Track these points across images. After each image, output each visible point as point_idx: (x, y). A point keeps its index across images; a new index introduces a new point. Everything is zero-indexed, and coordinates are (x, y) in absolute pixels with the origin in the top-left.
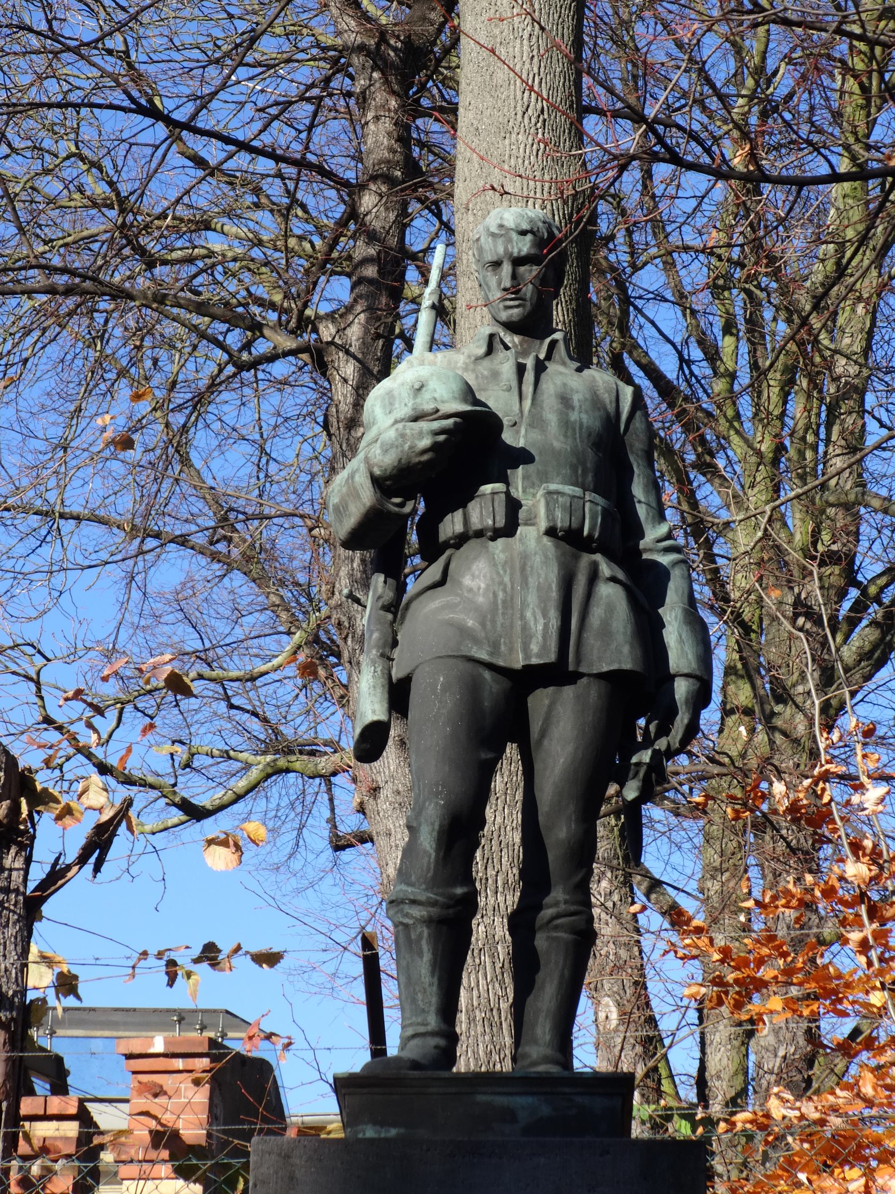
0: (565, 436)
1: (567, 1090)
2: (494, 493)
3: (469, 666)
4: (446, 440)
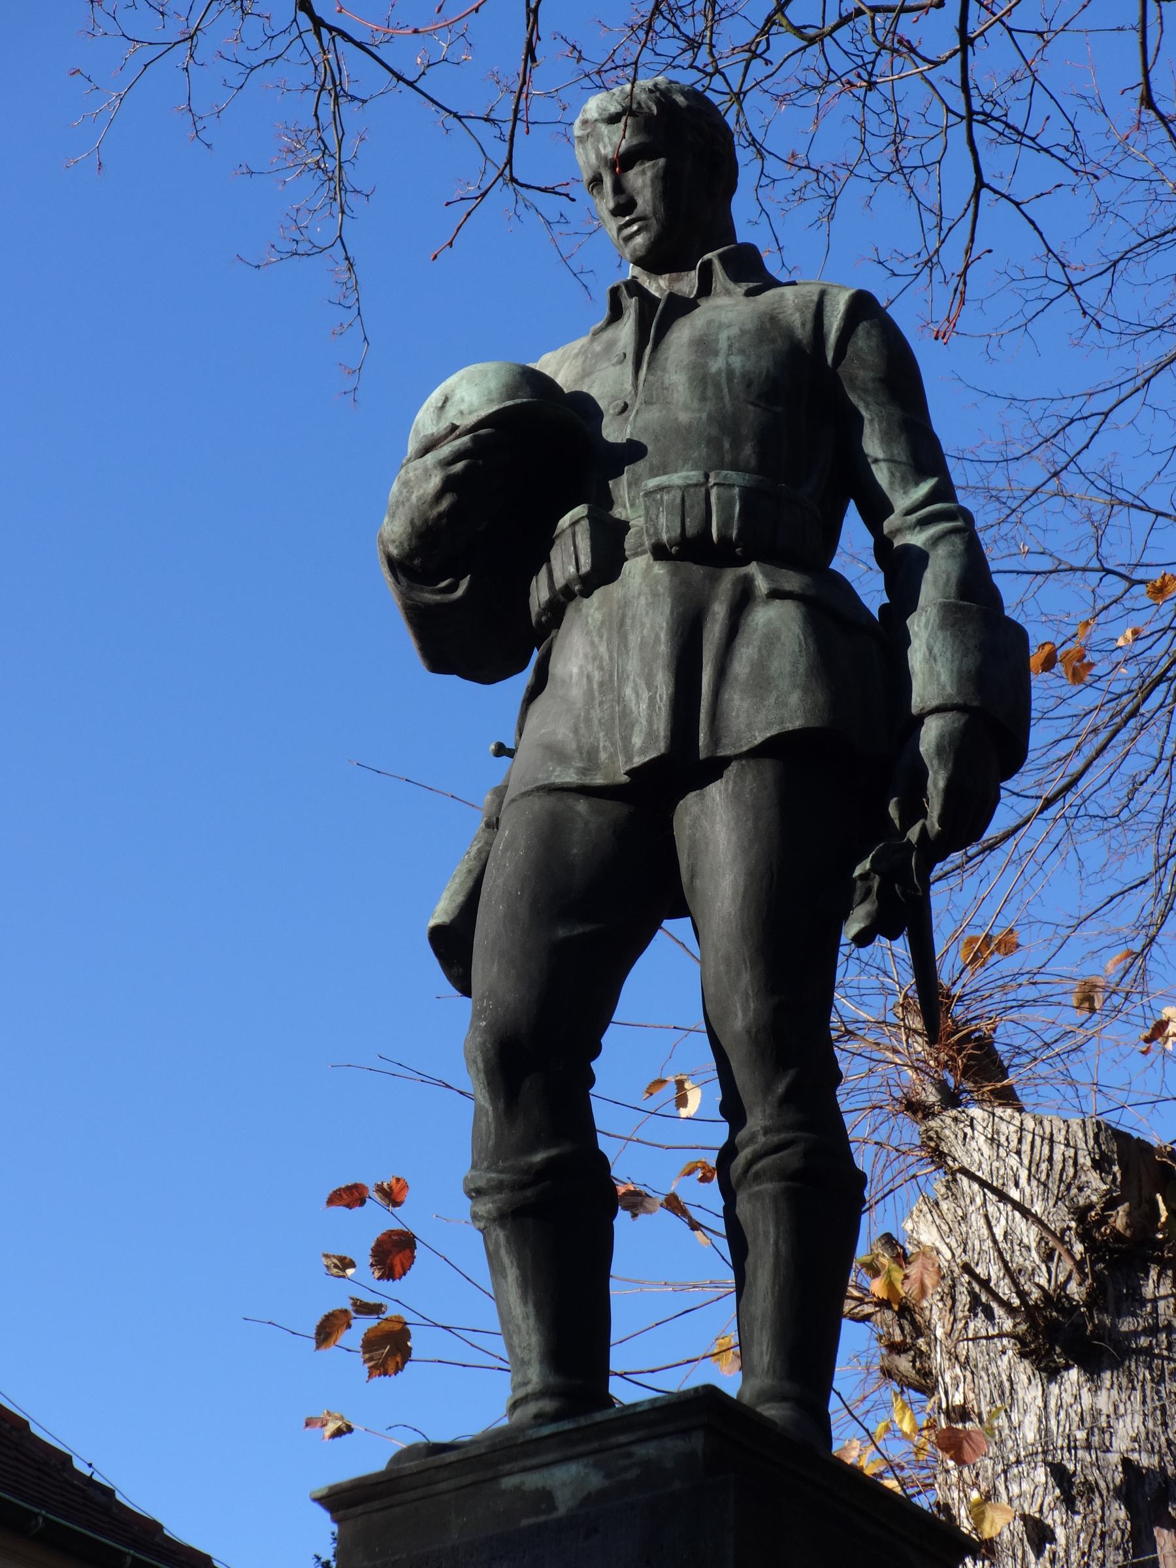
0: (703, 398)
1: (622, 1439)
2: (574, 524)
3: (549, 802)
4: (466, 467)
